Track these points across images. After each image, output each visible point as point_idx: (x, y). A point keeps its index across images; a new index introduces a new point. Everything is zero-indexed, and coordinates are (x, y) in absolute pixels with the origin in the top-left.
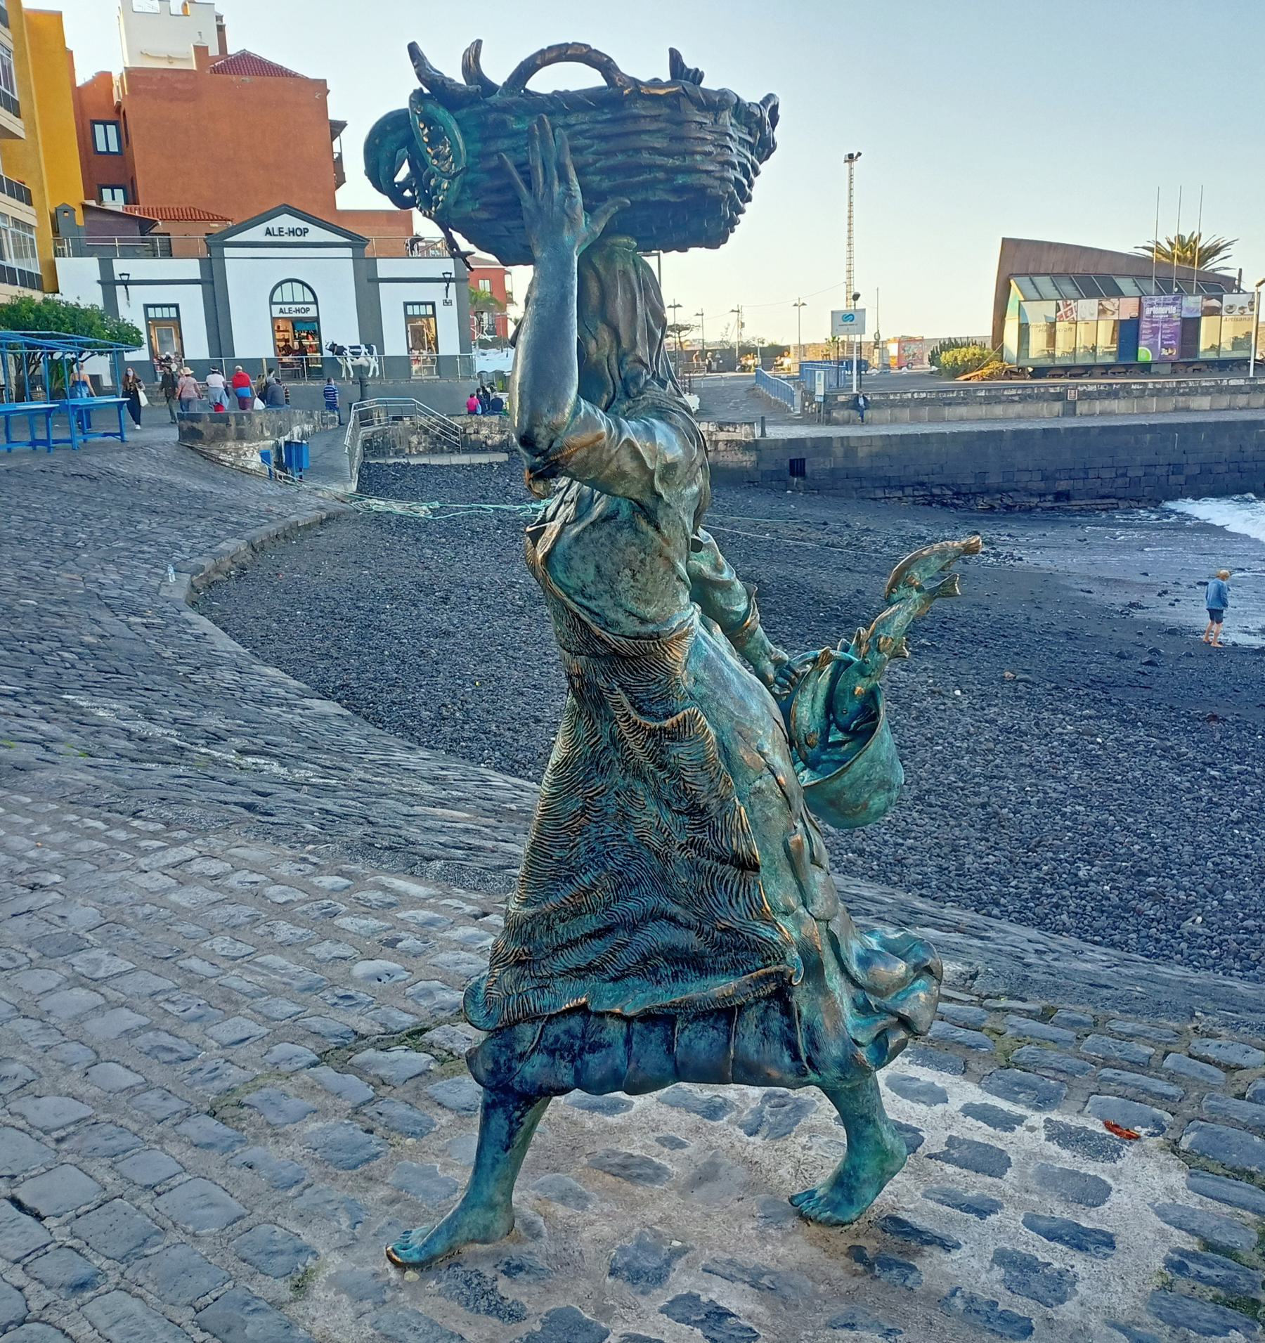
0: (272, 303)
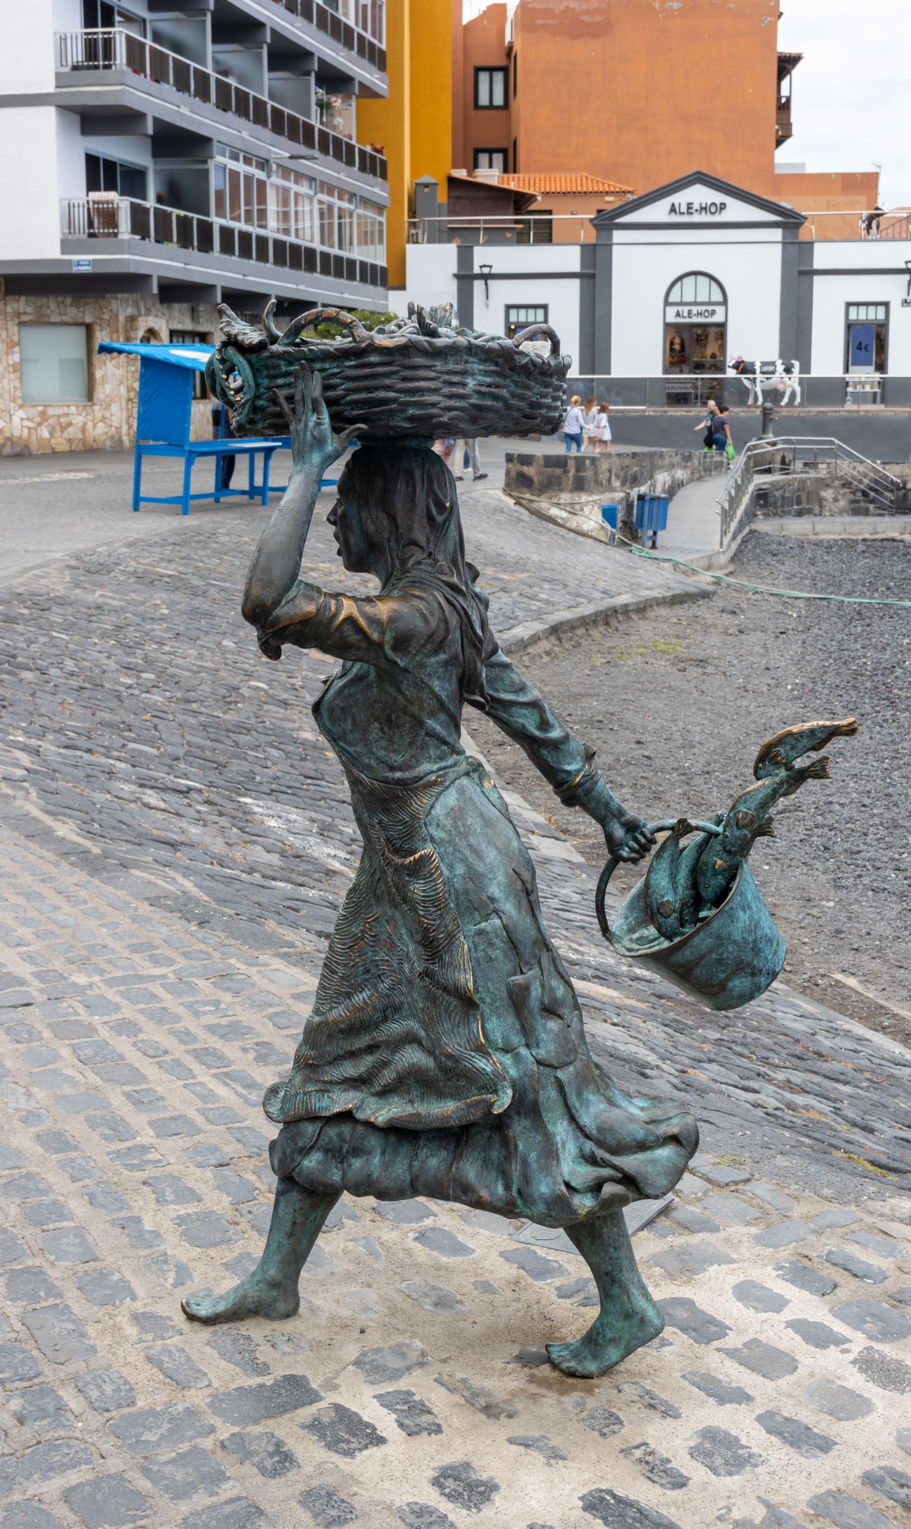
0: (667, 303)
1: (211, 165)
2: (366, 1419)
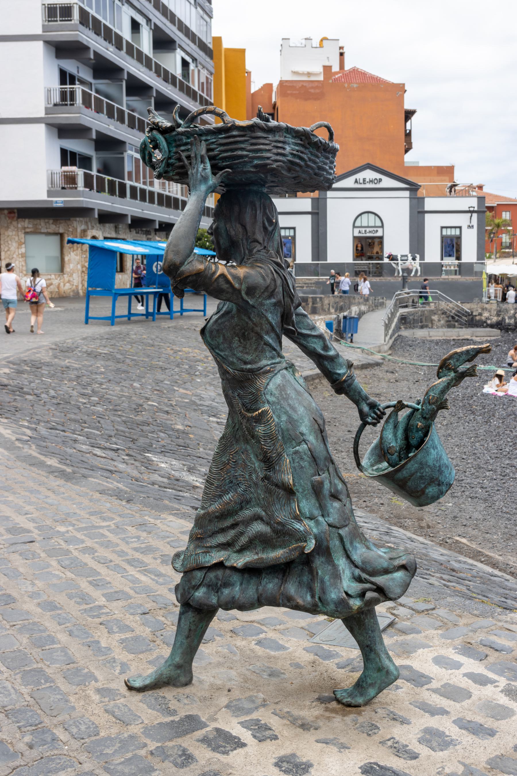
0: (354, 227)
1: (125, 155)
2: (234, 734)
